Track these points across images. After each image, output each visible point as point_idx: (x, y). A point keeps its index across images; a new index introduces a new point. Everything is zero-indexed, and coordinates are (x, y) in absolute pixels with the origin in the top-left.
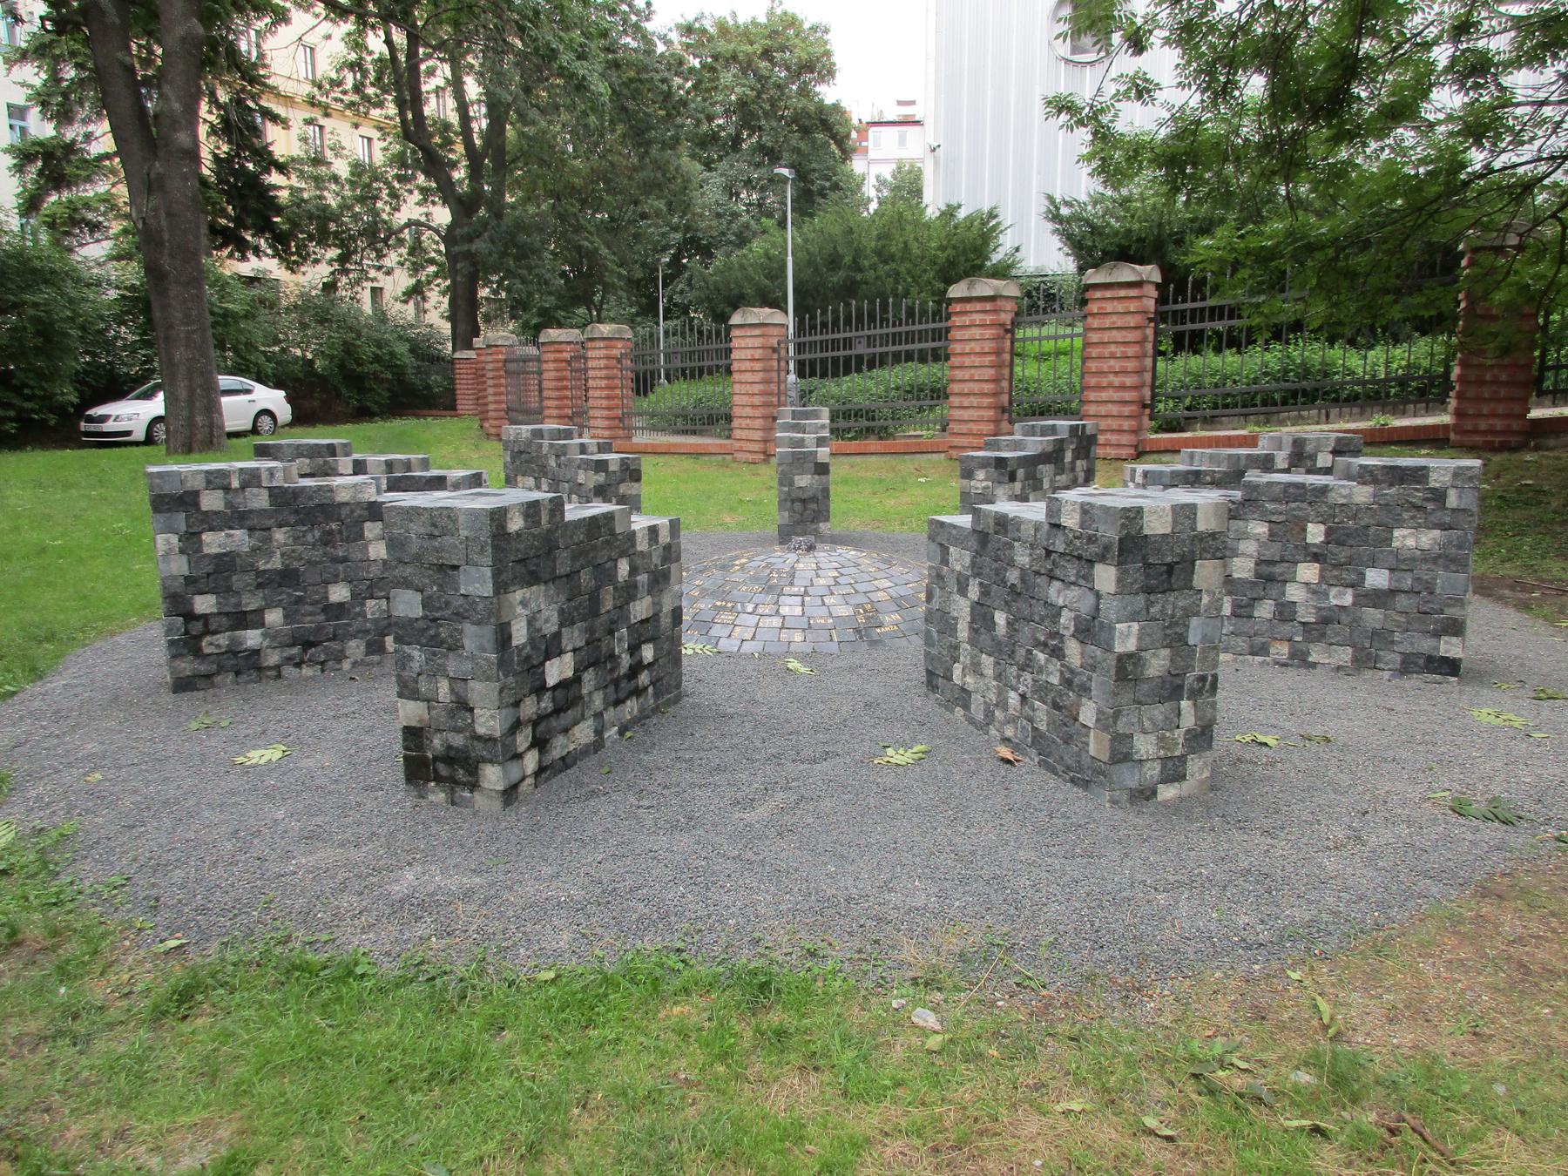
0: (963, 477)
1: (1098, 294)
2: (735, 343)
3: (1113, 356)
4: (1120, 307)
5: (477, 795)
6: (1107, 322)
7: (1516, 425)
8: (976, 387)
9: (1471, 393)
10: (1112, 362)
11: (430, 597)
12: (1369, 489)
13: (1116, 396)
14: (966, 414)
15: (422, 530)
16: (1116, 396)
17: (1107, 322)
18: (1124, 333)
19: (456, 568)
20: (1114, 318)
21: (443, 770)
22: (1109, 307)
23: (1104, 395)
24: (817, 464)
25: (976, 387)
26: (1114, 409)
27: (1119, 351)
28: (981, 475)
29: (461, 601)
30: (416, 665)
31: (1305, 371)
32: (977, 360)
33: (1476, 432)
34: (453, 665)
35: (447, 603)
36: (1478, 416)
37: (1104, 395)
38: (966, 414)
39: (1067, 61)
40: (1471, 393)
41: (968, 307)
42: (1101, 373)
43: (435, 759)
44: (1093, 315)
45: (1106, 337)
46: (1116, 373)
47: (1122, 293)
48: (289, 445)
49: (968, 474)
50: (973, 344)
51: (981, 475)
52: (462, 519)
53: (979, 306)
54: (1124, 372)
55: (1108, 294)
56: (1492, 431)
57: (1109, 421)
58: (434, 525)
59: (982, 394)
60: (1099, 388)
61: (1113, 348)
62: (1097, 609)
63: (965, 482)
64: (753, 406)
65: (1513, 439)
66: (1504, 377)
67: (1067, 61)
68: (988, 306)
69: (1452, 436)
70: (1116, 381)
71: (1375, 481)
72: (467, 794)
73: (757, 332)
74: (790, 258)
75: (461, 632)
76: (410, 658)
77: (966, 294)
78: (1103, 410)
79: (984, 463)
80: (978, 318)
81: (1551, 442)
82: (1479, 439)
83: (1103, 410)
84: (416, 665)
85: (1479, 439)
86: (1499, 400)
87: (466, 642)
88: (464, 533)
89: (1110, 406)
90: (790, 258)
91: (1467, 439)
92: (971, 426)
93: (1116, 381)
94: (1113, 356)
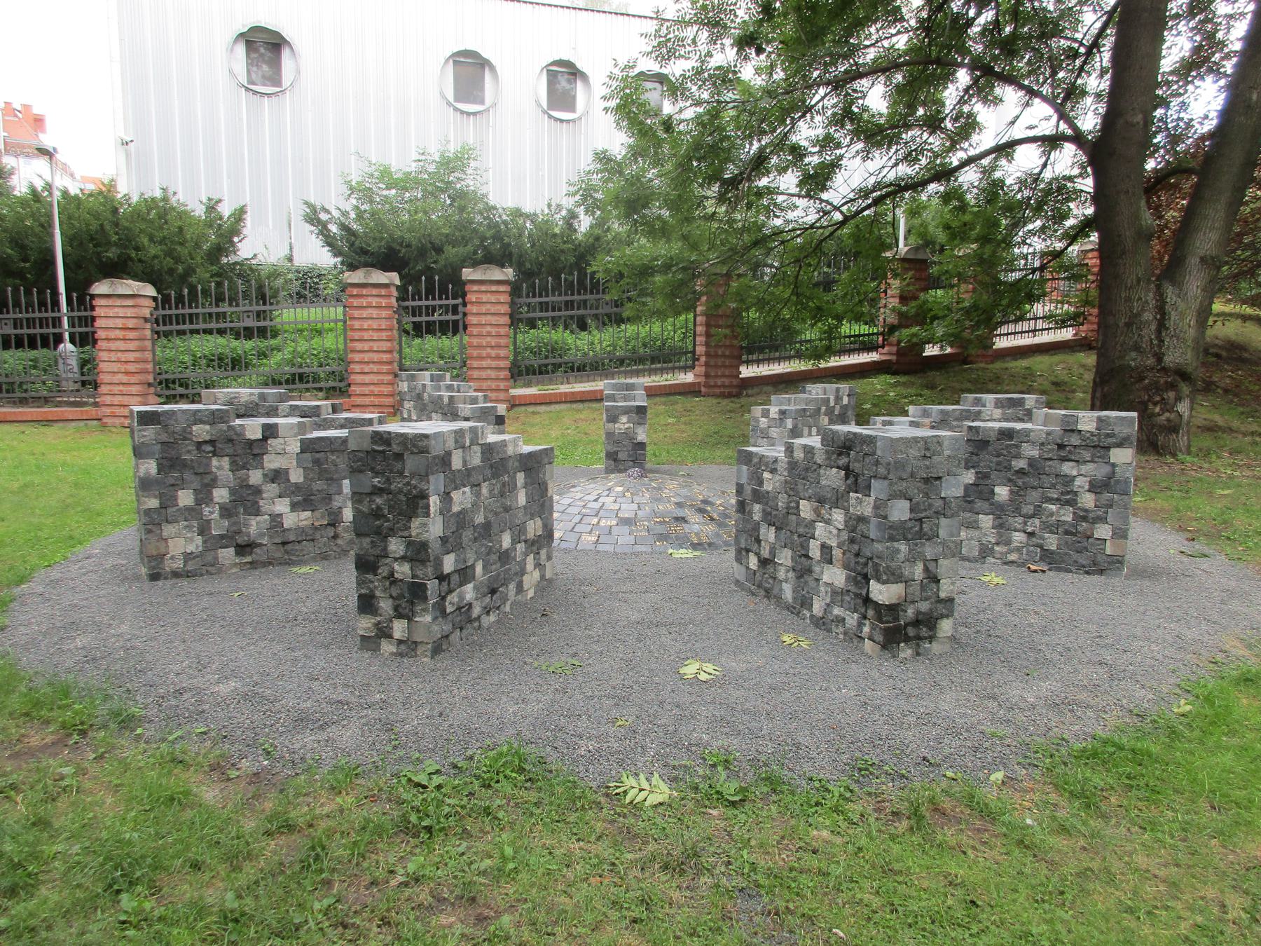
0: (609, 421)
1: (475, 288)
2: (98, 312)
3: (489, 334)
4: (493, 298)
5: (934, 644)
6: (484, 309)
7: (735, 382)
8: (376, 357)
9: (712, 362)
10: (489, 339)
11: (918, 503)
12: (1000, 411)
13: (494, 364)
14: (367, 379)
15: (917, 454)
16: (494, 364)
17: (484, 309)
18: (496, 318)
19: (939, 478)
20: (488, 306)
21: (911, 631)
22: (485, 298)
23: (484, 363)
24: (498, 417)
25: (376, 357)
26: (493, 374)
27: (493, 331)
28: (624, 419)
29: (940, 502)
30: (901, 556)
31: (553, 349)
32: (375, 335)
33: (716, 386)
34: (929, 551)
35: (930, 505)
36: (716, 376)
37: (484, 363)
38: (367, 379)
39: (247, 89)
40: (712, 362)
41: (364, 292)
42: (480, 347)
43: (906, 625)
44: (472, 303)
45: (483, 320)
46: (492, 347)
47: (494, 288)
48: (184, 412)
49: (613, 419)
50: (370, 322)
51: (624, 419)
52: (946, 443)
53: (375, 291)
54: (498, 346)
55: (483, 288)
56: (723, 386)
57: (489, 383)
58: (927, 449)
59: (381, 363)
60: (481, 358)
61: (489, 329)
62: (1114, 473)
63: (610, 425)
64: (127, 373)
65: (734, 391)
66: (727, 353)
67: (449, 104)
68: (383, 292)
69: (703, 389)
70: (493, 353)
71: (1003, 407)
72: (927, 645)
73: (130, 302)
74: (57, 232)
75: (938, 526)
76: (898, 551)
77: (363, 281)
78: (484, 374)
79: (627, 411)
80: (374, 301)
81: (750, 392)
82: (717, 391)
83: (484, 374)
84: (901, 556)
85: (717, 391)
86: (725, 367)
87: (941, 532)
88: (947, 453)
89: (489, 372)
90: (57, 232)
91: (712, 391)
92: (372, 388)
93: (493, 353)
94: (489, 334)
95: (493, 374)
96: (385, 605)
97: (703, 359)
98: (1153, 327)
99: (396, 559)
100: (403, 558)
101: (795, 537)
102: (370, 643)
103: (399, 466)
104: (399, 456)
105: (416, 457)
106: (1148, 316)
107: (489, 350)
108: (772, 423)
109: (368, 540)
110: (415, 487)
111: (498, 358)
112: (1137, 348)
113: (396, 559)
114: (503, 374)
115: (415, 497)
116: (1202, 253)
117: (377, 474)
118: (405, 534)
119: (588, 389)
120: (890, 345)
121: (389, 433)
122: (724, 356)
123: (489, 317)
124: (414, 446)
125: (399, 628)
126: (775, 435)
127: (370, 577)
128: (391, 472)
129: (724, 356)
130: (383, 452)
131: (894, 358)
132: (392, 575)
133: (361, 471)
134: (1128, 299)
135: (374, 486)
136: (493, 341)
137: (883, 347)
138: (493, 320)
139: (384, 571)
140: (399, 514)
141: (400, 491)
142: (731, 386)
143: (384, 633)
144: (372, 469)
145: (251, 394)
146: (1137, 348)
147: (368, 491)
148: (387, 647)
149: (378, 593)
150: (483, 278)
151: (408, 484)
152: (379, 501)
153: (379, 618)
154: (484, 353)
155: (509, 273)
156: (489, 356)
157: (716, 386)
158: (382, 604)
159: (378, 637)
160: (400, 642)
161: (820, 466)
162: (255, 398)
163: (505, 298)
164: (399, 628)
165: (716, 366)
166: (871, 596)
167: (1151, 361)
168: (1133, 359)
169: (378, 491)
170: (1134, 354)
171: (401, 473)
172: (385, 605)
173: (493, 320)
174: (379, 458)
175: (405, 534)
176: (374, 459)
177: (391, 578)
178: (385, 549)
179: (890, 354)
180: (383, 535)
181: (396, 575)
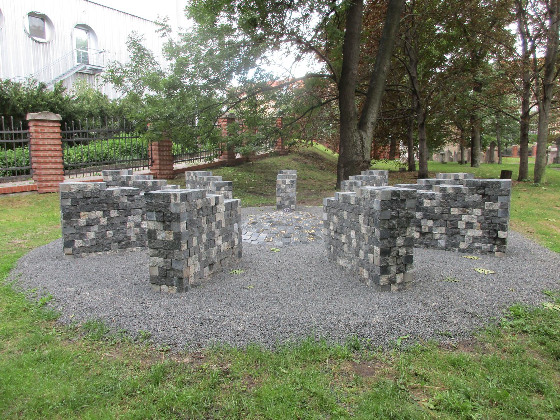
3: (50, 150)
4: (51, 130)
7: (172, 172)
10: (50, 153)
20: (48, 134)
22: (46, 130)
23: (48, 166)
27: (53, 148)
33: (164, 174)
37: (48, 166)
42: (45, 157)
46: (52, 157)
47: (51, 124)
51: (223, 189)
52: (502, 184)
55: (45, 124)
56: (167, 174)
57: (51, 177)
61: (49, 147)
65: (171, 176)
69: (158, 176)
70: (53, 160)
86: (167, 165)
89: (51, 171)
93: (53, 160)
94: (50, 150)
95: (54, 172)
96: (393, 269)
97: (157, 162)
98: (361, 146)
99: (399, 247)
100: (403, 246)
101: (448, 222)
102: (386, 288)
103: (403, 205)
104: (403, 201)
105: (411, 201)
106: (359, 142)
107: (50, 159)
108: (288, 186)
109: (386, 241)
110: (410, 214)
111: (56, 163)
112: (356, 154)
113: (399, 247)
114: (59, 172)
115: (410, 218)
116: (372, 121)
117: (393, 210)
118: (404, 235)
119: (24, 182)
120: (224, 154)
121: (399, 191)
122: (166, 160)
123: (49, 140)
124: (411, 196)
125: (399, 278)
126: (289, 191)
127: (387, 257)
128: (400, 208)
129: (166, 160)
130: (396, 200)
131: (227, 160)
132: (398, 254)
133: (386, 210)
134: (353, 136)
135: (393, 216)
136: (53, 154)
137: (221, 155)
138: (52, 142)
139: (393, 253)
140: (402, 227)
141: (404, 216)
142: (170, 174)
143: (392, 281)
144: (391, 208)
145: (95, 185)
146: (356, 154)
147: (389, 218)
148: (394, 287)
149: (390, 264)
150: (45, 119)
151: (407, 213)
152: (394, 222)
153: (390, 275)
154: (48, 160)
155: (58, 117)
156: (51, 162)
157: (164, 174)
158: (392, 269)
159: (390, 284)
160: (400, 284)
161: (465, 194)
162: (99, 187)
163: (58, 130)
164: (399, 278)
165: (164, 165)
166: (499, 236)
167: (361, 159)
168: (355, 158)
169: (393, 217)
170: (355, 156)
171: (404, 208)
172: (393, 269)
173: (52, 142)
174: (394, 202)
175: (404, 235)
176: (392, 203)
177: (397, 256)
178: (395, 243)
179: (224, 158)
180: (394, 237)
181: (400, 254)
